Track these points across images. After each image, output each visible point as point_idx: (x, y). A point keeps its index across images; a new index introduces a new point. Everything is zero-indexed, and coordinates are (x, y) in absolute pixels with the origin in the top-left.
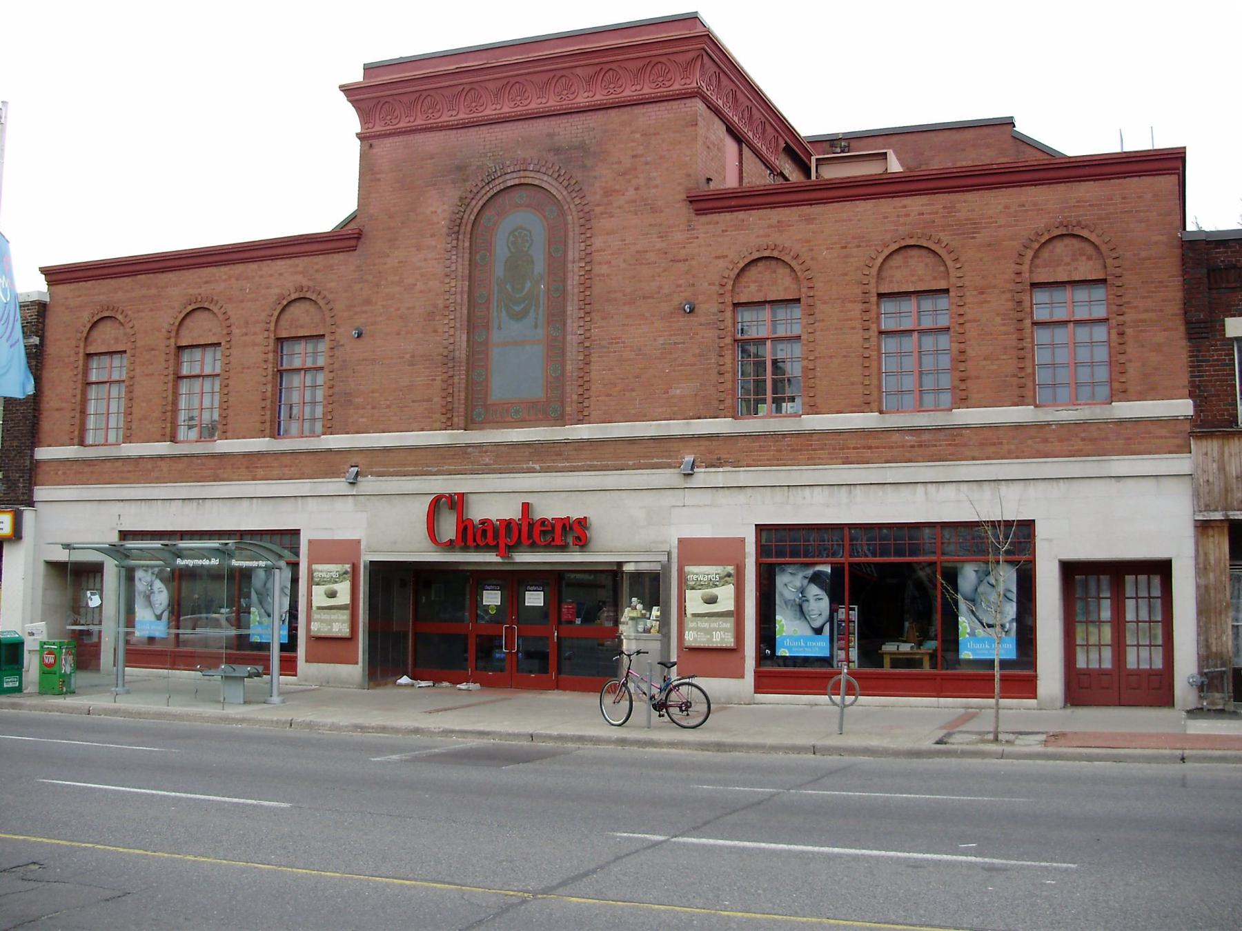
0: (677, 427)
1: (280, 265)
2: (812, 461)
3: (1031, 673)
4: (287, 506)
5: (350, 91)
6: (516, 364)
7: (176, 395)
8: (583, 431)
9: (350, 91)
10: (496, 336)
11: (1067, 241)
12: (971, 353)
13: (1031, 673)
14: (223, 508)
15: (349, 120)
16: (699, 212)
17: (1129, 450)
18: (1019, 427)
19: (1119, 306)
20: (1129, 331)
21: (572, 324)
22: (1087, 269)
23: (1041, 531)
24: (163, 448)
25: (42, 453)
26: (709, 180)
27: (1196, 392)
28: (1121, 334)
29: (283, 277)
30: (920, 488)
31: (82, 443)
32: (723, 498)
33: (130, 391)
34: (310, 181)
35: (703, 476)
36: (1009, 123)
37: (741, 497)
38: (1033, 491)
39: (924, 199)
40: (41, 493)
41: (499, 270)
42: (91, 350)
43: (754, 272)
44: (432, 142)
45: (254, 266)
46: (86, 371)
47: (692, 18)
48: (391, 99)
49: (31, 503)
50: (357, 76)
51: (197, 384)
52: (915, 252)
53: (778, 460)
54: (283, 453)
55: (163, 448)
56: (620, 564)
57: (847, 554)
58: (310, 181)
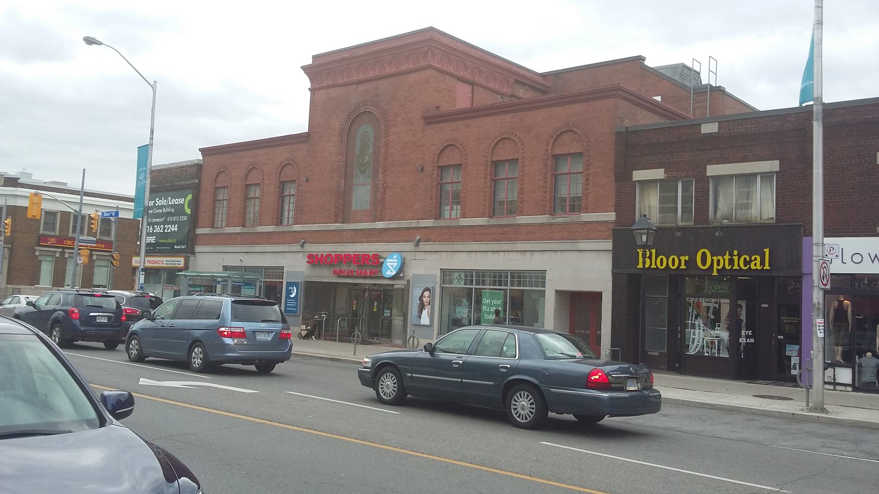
0: (413, 223)
1: (282, 148)
2: (463, 240)
3: (59, 214)
4: (280, 256)
5: (305, 69)
6: (362, 195)
7: (245, 206)
8: (380, 225)
9: (305, 69)
10: (355, 181)
11: (569, 133)
12: (525, 189)
13: (59, 214)
14: (258, 256)
15: (305, 82)
16: (428, 124)
17: (587, 238)
18: (542, 225)
19: (587, 167)
20: (590, 178)
21: (380, 176)
22: (575, 148)
23: (548, 276)
24: (238, 230)
25: (199, 231)
26: (438, 107)
27: (618, 210)
28: (587, 180)
29: (282, 154)
30: (502, 253)
31: (213, 227)
32: (429, 256)
33: (229, 204)
34: (287, 111)
35: (423, 246)
36: (640, 59)
37: (436, 256)
38: (547, 255)
39: (511, 115)
40: (198, 249)
41: (357, 151)
42: (217, 185)
43: (446, 152)
44: (334, 92)
45: (272, 149)
46: (215, 195)
47: (431, 29)
48: (325, 71)
49: (194, 253)
50: (309, 61)
51: (253, 200)
52: (507, 141)
53: (450, 240)
54: (280, 232)
55: (238, 230)
56: (853, 391)
57: (463, 282)
58: (287, 111)
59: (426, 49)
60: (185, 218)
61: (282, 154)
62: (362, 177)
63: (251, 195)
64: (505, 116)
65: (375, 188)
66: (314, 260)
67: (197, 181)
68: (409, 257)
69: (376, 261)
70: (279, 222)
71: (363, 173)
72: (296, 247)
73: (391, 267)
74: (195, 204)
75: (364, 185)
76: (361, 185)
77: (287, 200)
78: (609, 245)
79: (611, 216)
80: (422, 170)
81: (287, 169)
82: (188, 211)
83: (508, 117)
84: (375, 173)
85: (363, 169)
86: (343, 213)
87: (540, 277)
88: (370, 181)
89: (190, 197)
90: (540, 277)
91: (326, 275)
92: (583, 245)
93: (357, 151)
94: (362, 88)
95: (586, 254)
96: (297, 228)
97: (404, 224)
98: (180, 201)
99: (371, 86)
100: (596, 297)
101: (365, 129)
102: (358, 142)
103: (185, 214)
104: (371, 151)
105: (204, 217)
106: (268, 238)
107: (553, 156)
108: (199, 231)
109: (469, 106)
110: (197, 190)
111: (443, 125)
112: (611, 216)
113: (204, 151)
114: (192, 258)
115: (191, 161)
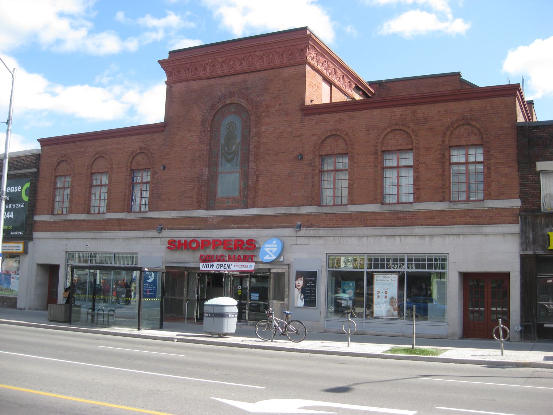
0: (293, 210)
5: (162, 63)
6: (229, 182)
9: (162, 63)
10: (220, 169)
16: (306, 115)
20: (492, 168)
21: (252, 164)
23: (450, 260)
24: (83, 217)
25: (37, 218)
27: (522, 196)
29: (134, 143)
31: (52, 214)
35: (303, 231)
39: (403, 109)
40: (36, 235)
41: (222, 141)
42: (57, 174)
45: (122, 139)
49: (31, 239)
50: (166, 57)
51: (98, 188)
55: (83, 217)
59: (243, 56)
60: (22, 205)
61: (134, 143)
62: (228, 165)
63: (138, 179)
64: (395, 109)
65: (245, 176)
66: (175, 245)
67: (35, 170)
68: (289, 242)
69: (250, 247)
70: (129, 209)
71: (229, 161)
72: (153, 233)
73: (269, 251)
74: (33, 192)
75: (232, 172)
76: (228, 172)
77: (138, 188)
78: (516, 228)
79: (516, 203)
80: (164, 169)
81: (139, 158)
82: (26, 198)
83: (399, 111)
84: (245, 161)
85: (229, 157)
86: (209, 201)
87: (439, 262)
88: (238, 168)
89: (28, 185)
90: (439, 262)
91: (186, 259)
92: (488, 229)
93: (222, 141)
94: (229, 80)
95: (491, 237)
96: (354, 208)
97: (281, 211)
98: (18, 189)
99: (241, 77)
100: (503, 278)
101: (232, 121)
102: (223, 132)
103: (22, 201)
104: (239, 140)
105: (41, 204)
106: (119, 225)
107: (320, 156)
108: (37, 218)
109: (329, 102)
110: (35, 179)
111: (324, 116)
112: (516, 203)
113: (43, 142)
114: (30, 244)
115: (30, 151)
